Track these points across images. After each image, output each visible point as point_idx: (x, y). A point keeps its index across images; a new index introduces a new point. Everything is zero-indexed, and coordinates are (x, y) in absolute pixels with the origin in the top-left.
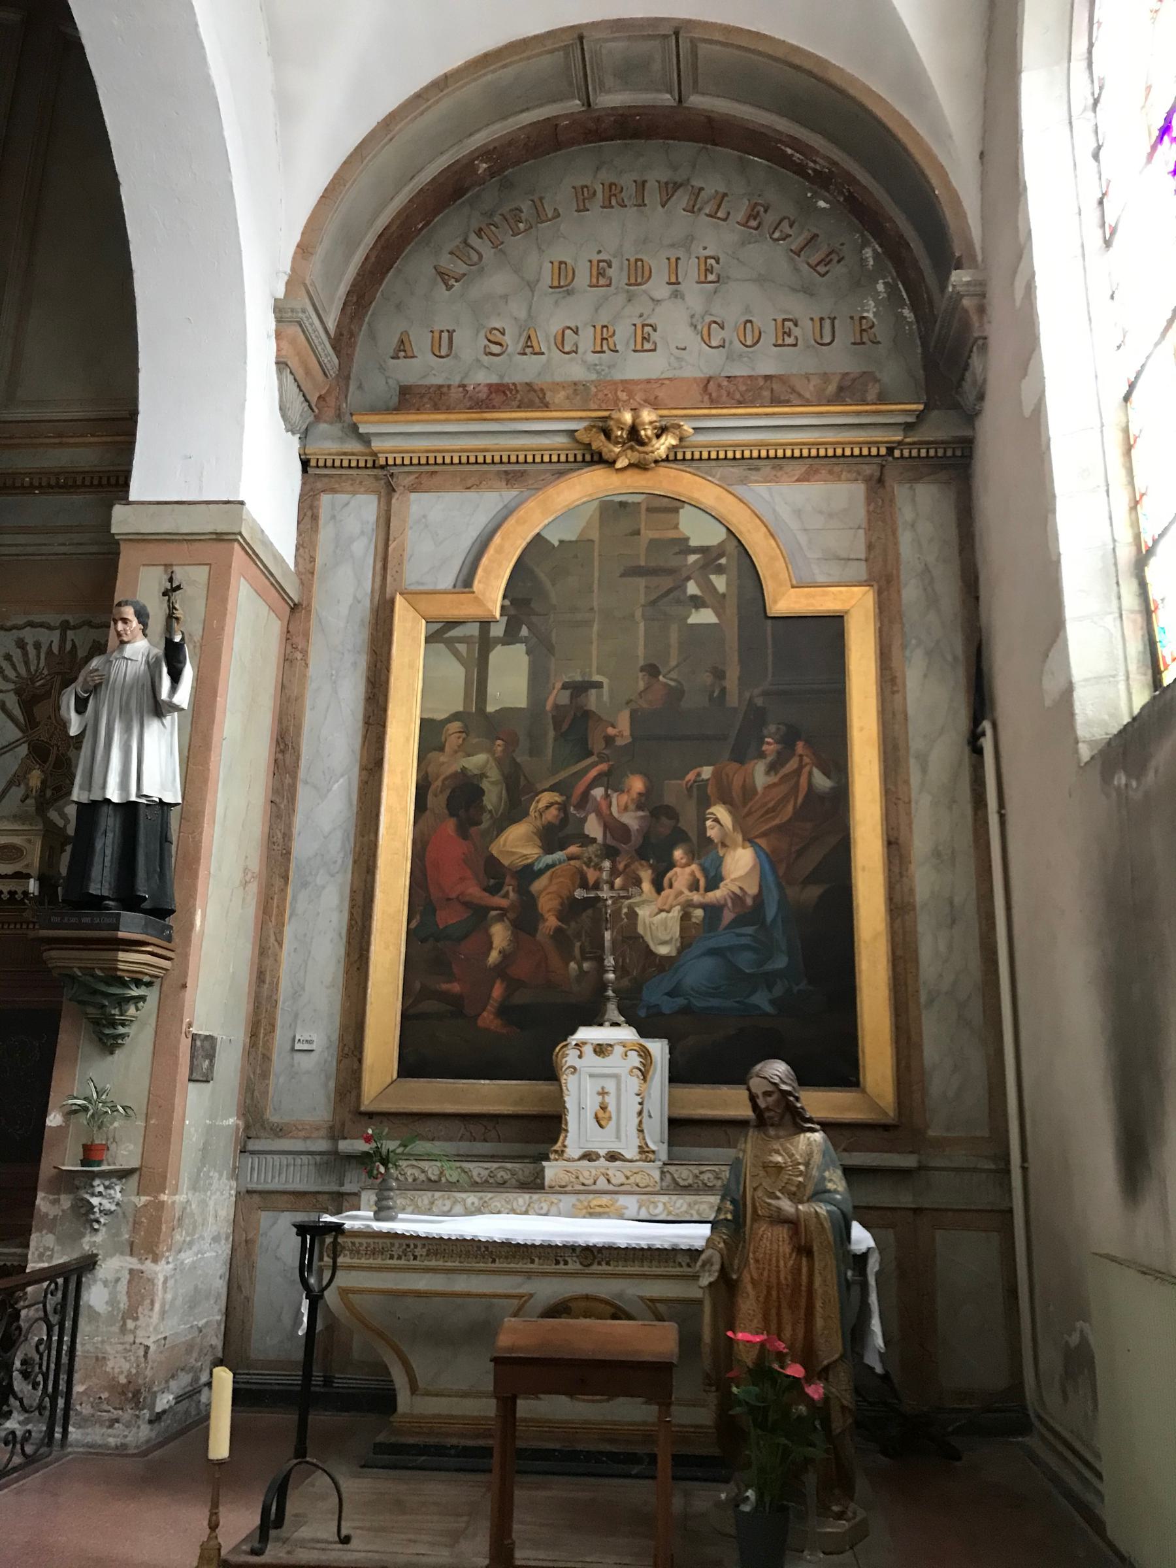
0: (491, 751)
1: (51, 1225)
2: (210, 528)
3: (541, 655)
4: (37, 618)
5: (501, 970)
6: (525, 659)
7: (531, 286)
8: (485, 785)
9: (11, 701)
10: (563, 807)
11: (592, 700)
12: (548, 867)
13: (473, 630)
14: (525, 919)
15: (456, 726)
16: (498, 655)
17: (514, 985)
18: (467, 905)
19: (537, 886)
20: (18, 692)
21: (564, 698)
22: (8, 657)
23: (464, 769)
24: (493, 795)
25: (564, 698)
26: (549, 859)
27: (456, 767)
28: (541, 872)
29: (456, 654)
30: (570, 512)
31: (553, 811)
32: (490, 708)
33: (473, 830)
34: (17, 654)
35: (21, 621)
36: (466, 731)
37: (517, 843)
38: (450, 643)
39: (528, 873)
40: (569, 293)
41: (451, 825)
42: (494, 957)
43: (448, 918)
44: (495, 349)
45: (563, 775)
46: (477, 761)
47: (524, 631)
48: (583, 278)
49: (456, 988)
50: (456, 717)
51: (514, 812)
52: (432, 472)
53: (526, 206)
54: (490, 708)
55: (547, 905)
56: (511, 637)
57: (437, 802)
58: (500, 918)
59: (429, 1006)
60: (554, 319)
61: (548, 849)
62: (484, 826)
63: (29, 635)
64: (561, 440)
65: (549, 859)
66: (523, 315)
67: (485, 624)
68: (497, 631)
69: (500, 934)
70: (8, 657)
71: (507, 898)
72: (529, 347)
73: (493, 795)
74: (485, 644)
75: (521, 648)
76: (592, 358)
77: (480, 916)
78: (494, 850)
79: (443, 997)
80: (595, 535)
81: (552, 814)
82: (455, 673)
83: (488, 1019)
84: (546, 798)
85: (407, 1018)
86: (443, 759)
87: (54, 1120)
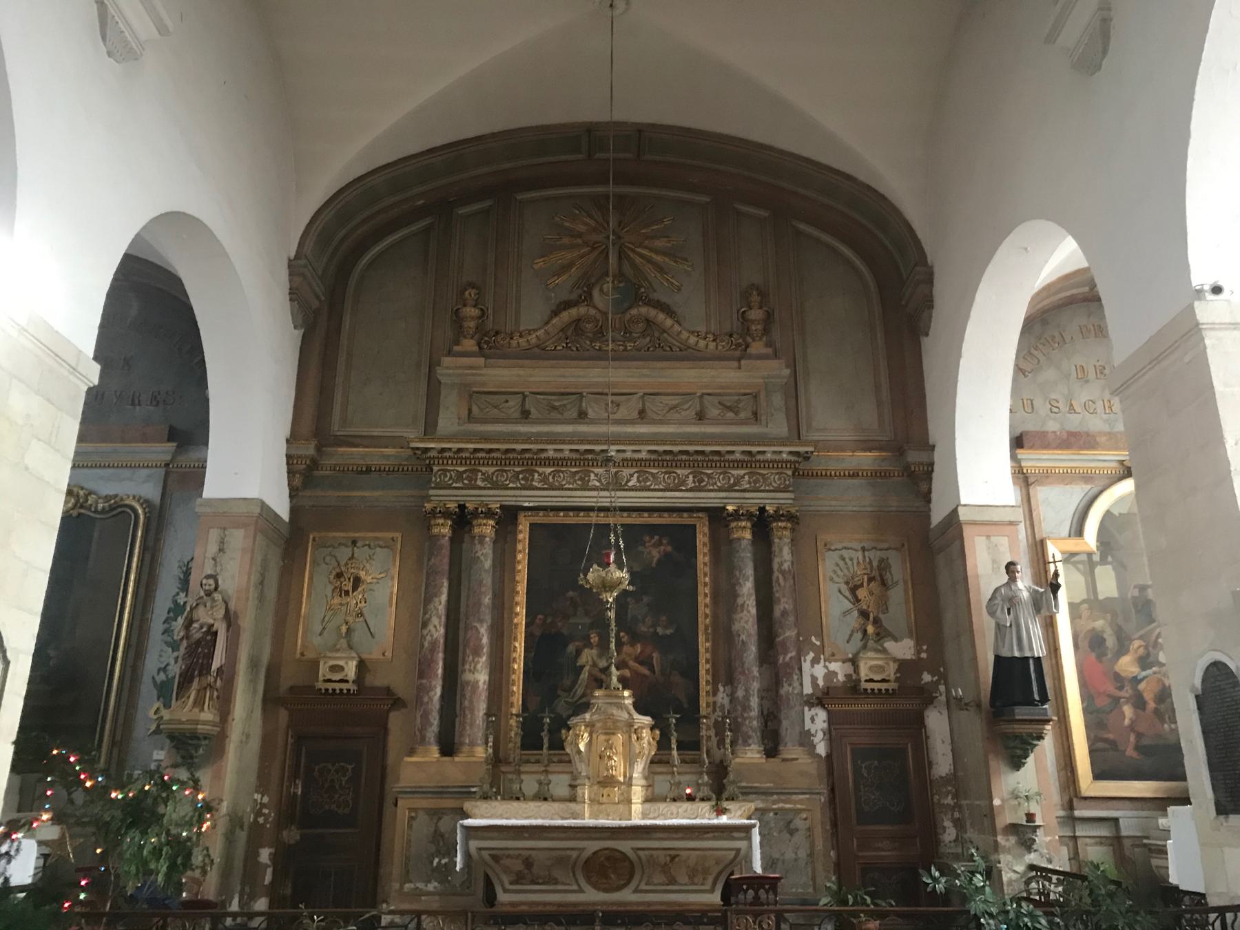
0: (1104, 618)
1: (1008, 851)
2: (1007, 519)
3: (1121, 569)
4: (850, 545)
5: (1132, 728)
6: (1112, 574)
7: (1068, 376)
8: (1105, 636)
9: (844, 588)
10: (1146, 647)
11: (1150, 593)
12: (1145, 678)
13: (1084, 557)
14: (1139, 702)
15: (1085, 606)
16: (1099, 570)
17: (1139, 736)
18: (1109, 696)
19: (1141, 686)
20: (847, 583)
21: (1136, 593)
22: (837, 565)
23: (1093, 629)
24: (1111, 641)
25: (1136, 593)
26: (1144, 674)
27: (1089, 627)
28: (1142, 680)
29: (1078, 569)
30: (1122, 499)
31: (1142, 649)
32: (1101, 597)
33: (1104, 659)
34: (841, 563)
35: (839, 546)
36: (1090, 608)
37: (1127, 665)
38: (1075, 564)
39: (1136, 681)
40: (1087, 381)
41: (1093, 656)
42: (1127, 722)
43: (1102, 702)
44: (1055, 410)
45: (1142, 632)
46: (1099, 624)
47: (1110, 559)
48: (1092, 375)
49: (1111, 736)
50: (1084, 601)
51: (1122, 650)
52: (1048, 477)
53: (1056, 334)
54: (1101, 597)
55: (1148, 696)
56: (1103, 561)
57: (1084, 644)
58: (1127, 703)
59: (1100, 745)
60: (1083, 395)
61: (1143, 669)
62: (1109, 656)
63: (845, 553)
64: (1115, 465)
65: (1144, 674)
66: (1066, 392)
67: (1090, 555)
68: (1096, 558)
69: (1128, 711)
70: (837, 565)
71: (1127, 692)
72: (1072, 409)
73: (1111, 641)
74: (1091, 565)
75: (1109, 567)
76: (1105, 416)
77: (1116, 701)
78: (1117, 668)
79: (1106, 740)
80: (1136, 510)
81: (1141, 651)
82: (1080, 579)
83: (1130, 752)
84: (1136, 643)
85: (1092, 751)
86: (1082, 622)
87: (997, 802)
